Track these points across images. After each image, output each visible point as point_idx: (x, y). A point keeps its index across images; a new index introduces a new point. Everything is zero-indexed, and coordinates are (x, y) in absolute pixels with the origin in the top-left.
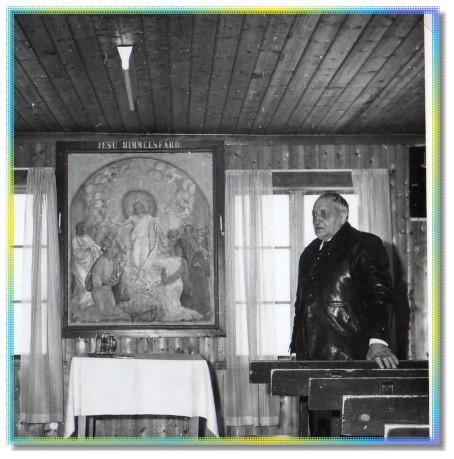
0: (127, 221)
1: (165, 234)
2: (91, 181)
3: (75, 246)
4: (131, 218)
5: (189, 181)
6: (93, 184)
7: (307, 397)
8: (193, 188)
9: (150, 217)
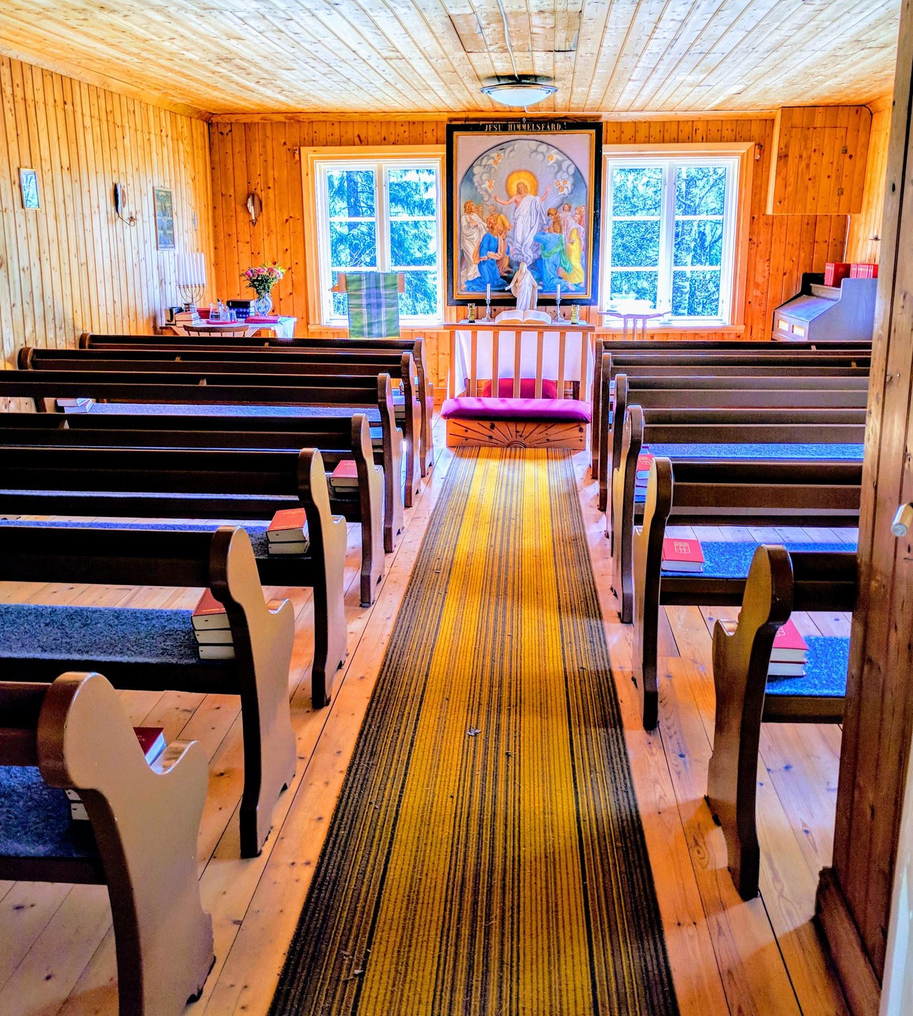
0: (512, 200)
1: (545, 212)
2: (478, 162)
3: (464, 223)
4: (514, 198)
5: (569, 162)
6: (480, 165)
7: (538, 305)
8: (572, 170)
9: (532, 197)
